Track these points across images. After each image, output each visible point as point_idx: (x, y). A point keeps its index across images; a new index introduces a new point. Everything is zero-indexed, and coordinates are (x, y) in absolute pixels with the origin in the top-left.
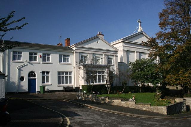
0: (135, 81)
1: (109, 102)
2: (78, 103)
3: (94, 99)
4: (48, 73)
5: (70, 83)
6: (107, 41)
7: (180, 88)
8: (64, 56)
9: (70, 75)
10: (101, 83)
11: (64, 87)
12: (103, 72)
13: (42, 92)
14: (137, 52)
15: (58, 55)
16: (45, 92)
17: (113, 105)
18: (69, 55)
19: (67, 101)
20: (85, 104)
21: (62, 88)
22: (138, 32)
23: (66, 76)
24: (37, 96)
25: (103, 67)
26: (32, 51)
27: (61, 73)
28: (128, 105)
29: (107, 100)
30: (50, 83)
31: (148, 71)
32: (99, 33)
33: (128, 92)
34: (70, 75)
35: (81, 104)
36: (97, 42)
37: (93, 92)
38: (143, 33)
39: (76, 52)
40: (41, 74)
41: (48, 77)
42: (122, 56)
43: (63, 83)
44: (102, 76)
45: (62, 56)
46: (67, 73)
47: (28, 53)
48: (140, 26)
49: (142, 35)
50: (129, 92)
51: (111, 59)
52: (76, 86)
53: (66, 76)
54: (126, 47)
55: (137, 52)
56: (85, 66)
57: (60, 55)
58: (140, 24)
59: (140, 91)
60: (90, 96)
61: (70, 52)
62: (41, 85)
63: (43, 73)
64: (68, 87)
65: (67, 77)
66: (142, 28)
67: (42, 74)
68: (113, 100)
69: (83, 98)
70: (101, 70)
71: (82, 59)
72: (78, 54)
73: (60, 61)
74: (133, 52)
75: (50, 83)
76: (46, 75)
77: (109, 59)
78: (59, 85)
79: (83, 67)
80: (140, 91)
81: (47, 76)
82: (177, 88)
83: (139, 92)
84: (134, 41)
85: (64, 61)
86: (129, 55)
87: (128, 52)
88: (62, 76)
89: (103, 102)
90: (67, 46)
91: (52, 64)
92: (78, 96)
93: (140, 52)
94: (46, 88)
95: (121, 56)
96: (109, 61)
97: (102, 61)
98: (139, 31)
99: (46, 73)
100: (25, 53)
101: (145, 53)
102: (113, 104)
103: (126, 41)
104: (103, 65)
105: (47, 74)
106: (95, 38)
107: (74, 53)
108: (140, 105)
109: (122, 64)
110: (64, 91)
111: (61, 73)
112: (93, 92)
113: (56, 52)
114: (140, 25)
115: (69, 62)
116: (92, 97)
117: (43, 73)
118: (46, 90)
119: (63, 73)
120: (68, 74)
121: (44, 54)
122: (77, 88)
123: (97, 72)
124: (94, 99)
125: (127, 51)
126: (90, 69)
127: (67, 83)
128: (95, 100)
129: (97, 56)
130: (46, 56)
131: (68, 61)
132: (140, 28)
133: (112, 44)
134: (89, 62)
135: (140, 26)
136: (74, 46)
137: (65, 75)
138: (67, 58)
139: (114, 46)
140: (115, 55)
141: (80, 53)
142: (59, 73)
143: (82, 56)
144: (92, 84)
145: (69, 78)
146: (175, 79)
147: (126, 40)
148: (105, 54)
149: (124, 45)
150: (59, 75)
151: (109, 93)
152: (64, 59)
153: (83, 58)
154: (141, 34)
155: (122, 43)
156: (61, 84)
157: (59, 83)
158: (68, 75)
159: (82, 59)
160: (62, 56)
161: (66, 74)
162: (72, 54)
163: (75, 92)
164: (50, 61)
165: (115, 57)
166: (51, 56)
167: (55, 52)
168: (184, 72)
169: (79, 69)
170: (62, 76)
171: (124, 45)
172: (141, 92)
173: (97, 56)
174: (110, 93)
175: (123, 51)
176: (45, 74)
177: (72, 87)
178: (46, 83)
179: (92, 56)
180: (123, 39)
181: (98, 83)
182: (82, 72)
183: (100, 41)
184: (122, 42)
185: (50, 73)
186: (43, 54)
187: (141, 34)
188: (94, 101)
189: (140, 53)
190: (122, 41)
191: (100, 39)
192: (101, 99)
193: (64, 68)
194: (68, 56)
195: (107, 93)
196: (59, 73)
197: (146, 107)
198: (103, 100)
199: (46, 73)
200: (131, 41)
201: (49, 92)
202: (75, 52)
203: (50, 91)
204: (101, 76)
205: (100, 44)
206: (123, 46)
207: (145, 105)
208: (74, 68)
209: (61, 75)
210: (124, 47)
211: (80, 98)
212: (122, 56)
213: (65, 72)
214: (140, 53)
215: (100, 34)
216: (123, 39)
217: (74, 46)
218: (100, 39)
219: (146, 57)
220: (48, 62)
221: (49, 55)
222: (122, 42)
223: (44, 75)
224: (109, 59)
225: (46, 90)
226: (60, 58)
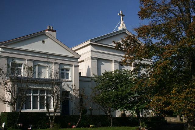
0: (104, 107)
10: (38, 110)
22: (119, 30)
31: (123, 91)
32: (48, 28)
33: (89, 126)
36: (43, 42)
37: (19, 125)
42: (90, 67)
44: (40, 97)
48: (122, 21)
50: (91, 126)
51: (68, 70)
54: (102, 54)
55: (115, 62)
56: (16, 81)
59: (112, 123)
66: (124, 25)
70: (38, 87)
71: (63, 73)
79: (12, 82)
80: (112, 123)
82: (135, 114)
84: (110, 45)
93: (99, 59)
95: (88, 66)
96: (63, 73)
98: (120, 28)
101: (109, 61)
103: (97, 43)
104: (47, 79)
106: (40, 35)
109: (90, 79)
112: (19, 125)
114: (122, 19)
123: (46, 91)
125: (99, 60)
126: (24, 86)
129: (42, 64)
132: (121, 25)
133: (74, 49)
134: (24, 73)
135: (122, 21)
140: (73, 64)
143: (63, 70)
146: (163, 103)
147: (97, 42)
155: (90, 46)
165: (73, 67)
168: (179, 92)
172: (113, 126)
173: (42, 64)
175: (92, 59)
179: (57, 67)
180: (91, 41)
181: (31, 110)
183: (47, 41)
184: (90, 44)
190: (89, 42)
191: (48, 37)
204: (39, 98)
206: (92, 51)
212: (90, 67)
215: (49, 30)
219: (112, 68)
222: (90, 44)
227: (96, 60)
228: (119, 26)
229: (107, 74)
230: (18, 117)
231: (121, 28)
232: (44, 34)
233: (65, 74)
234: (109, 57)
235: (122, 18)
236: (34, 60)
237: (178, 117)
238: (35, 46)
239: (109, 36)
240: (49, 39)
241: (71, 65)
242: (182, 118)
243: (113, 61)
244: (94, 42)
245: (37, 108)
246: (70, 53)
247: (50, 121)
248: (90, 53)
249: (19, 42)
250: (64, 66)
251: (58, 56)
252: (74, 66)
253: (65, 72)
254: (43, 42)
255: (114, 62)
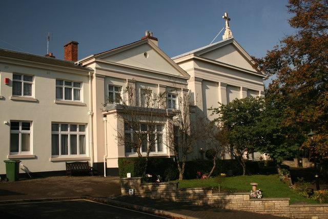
1: (217, 202)
2: (135, 207)
3: (173, 195)
4: (26, 125)
5: (83, 152)
6: (167, 56)
7: (306, 164)
8: (68, 83)
9: (82, 133)
11: (67, 164)
12: (160, 127)
13: (11, 177)
14: (222, 84)
15: (54, 81)
16: (19, 177)
17: (229, 211)
18: (80, 81)
19: (99, 201)
20: (161, 211)
21: (62, 167)
23: (72, 136)
24: (124, 196)
25: (160, 114)
26: (61, 76)
27: (60, 128)
28: (270, 208)
29: (212, 197)
30: (31, 153)
32: (146, 35)
34: (82, 133)
35: (146, 212)
36: (145, 55)
37: (149, 176)
38: (235, 43)
39: (97, 76)
40: (9, 128)
41: (26, 137)
43: (64, 152)
45: (64, 83)
46: (74, 127)
47: (55, 80)
49: (231, 48)
51: (174, 96)
52: (96, 161)
53: (72, 136)
55: (222, 84)
56: (122, 111)
57: (59, 82)
58: (227, 22)
59: (244, 171)
60: (162, 187)
61: (81, 75)
62: (7, 157)
63: (14, 125)
64: (77, 163)
65: (73, 137)
67: (12, 129)
68: (228, 198)
69: (142, 192)
72: (102, 81)
73: (59, 95)
74: (215, 83)
75: (31, 153)
76: (21, 131)
77: (169, 96)
78: (54, 159)
80: (244, 171)
81: (23, 135)
82: (300, 164)
83: (242, 174)
84: (217, 60)
85: (68, 97)
86: (207, 91)
87: (204, 82)
88: (62, 135)
89: (200, 202)
90: (69, 59)
91: (37, 102)
92: (127, 188)
93: (204, 80)
94: (22, 165)
97: (154, 102)
98: (226, 36)
99: (20, 127)
100: (39, 78)
101: (237, 88)
102: (227, 207)
103: (201, 59)
105: (23, 129)
106: (141, 45)
107: (92, 77)
108: (302, 209)
110: (68, 175)
111: (60, 128)
112: (149, 176)
113: (47, 73)
114: (227, 25)
115: (79, 100)
116: (166, 190)
117: (14, 125)
118: (21, 172)
119: (65, 126)
120: (78, 129)
121: (15, 76)
122: (99, 167)
124: (173, 195)
127: (74, 152)
128: (177, 196)
130: (23, 82)
131: (77, 97)
133: (177, 62)
136: (94, 60)
137: (69, 132)
138: (74, 90)
139: (180, 65)
140: (182, 87)
141: (106, 77)
142: (55, 126)
143: (111, 87)
144: (144, 154)
145: (80, 139)
147: (201, 56)
148: (131, 78)
149: (198, 67)
150: (55, 133)
151: (181, 176)
152: (68, 91)
153: (114, 92)
154: (229, 45)
156: (61, 157)
157: (55, 152)
158: (78, 133)
159: (111, 94)
160: (64, 83)
161: (71, 131)
162: (86, 78)
163: (95, 175)
164: (33, 96)
166: (34, 82)
167: (46, 72)
169: (104, 119)
170: (62, 135)
171: (198, 67)
172: (247, 174)
174: (183, 179)
175: (196, 80)
176: (18, 129)
177: (88, 163)
178: (21, 154)
182: (113, 123)
183: (150, 53)
184: (193, 59)
185: (32, 128)
186: (13, 75)
187: (229, 45)
188: (174, 198)
189: (229, 88)
190: (192, 56)
191: (152, 48)
192: (195, 193)
193: (66, 114)
194: (78, 84)
195: (178, 177)
196: (55, 126)
197: (319, 212)
198: (201, 197)
199: (20, 127)
200: (210, 58)
201: (29, 178)
202: (94, 75)
203: (32, 174)
205: (149, 61)
207: (318, 209)
208: (92, 116)
209: (60, 133)
210: (196, 71)
211: (131, 192)
213: (60, 125)
214: (249, 91)
215: (149, 37)
216: (195, 54)
217: (94, 60)
218: (152, 48)
219: (241, 95)
220: (26, 96)
221: (30, 78)
222: (193, 59)
223: (15, 132)
224: (169, 96)
225: (21, 172)
226: (56, 87)
227: (200, 81)
228: (223, 33)
229: (237, 102)
230: (146, 165)
231: (228, 37)
232: (147, 44)
233: (172, 102)
234: (215, 78)
235: (228, 23)
236: (107, 77)
237: (296, 160)
238: (135, 61)
239: (220, 46)
240: (152, 50)
241: (177, 89)
242: (301, 162)
243: (241, 88)
244: (198, 56)
245: (155, 151)
246: (177, 72)
247: (180, 170)
248: (193, 71)
249: (119, 53)
250: (112, 81)
251: (130, 68)
252: (160, 87)
253: (172, 99)
254: (145, 55)
255: (243, 90)
